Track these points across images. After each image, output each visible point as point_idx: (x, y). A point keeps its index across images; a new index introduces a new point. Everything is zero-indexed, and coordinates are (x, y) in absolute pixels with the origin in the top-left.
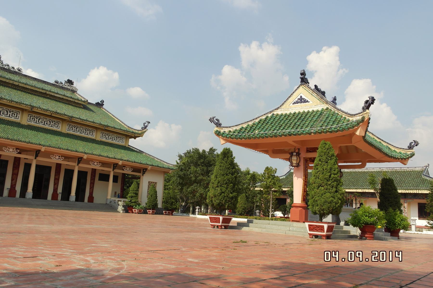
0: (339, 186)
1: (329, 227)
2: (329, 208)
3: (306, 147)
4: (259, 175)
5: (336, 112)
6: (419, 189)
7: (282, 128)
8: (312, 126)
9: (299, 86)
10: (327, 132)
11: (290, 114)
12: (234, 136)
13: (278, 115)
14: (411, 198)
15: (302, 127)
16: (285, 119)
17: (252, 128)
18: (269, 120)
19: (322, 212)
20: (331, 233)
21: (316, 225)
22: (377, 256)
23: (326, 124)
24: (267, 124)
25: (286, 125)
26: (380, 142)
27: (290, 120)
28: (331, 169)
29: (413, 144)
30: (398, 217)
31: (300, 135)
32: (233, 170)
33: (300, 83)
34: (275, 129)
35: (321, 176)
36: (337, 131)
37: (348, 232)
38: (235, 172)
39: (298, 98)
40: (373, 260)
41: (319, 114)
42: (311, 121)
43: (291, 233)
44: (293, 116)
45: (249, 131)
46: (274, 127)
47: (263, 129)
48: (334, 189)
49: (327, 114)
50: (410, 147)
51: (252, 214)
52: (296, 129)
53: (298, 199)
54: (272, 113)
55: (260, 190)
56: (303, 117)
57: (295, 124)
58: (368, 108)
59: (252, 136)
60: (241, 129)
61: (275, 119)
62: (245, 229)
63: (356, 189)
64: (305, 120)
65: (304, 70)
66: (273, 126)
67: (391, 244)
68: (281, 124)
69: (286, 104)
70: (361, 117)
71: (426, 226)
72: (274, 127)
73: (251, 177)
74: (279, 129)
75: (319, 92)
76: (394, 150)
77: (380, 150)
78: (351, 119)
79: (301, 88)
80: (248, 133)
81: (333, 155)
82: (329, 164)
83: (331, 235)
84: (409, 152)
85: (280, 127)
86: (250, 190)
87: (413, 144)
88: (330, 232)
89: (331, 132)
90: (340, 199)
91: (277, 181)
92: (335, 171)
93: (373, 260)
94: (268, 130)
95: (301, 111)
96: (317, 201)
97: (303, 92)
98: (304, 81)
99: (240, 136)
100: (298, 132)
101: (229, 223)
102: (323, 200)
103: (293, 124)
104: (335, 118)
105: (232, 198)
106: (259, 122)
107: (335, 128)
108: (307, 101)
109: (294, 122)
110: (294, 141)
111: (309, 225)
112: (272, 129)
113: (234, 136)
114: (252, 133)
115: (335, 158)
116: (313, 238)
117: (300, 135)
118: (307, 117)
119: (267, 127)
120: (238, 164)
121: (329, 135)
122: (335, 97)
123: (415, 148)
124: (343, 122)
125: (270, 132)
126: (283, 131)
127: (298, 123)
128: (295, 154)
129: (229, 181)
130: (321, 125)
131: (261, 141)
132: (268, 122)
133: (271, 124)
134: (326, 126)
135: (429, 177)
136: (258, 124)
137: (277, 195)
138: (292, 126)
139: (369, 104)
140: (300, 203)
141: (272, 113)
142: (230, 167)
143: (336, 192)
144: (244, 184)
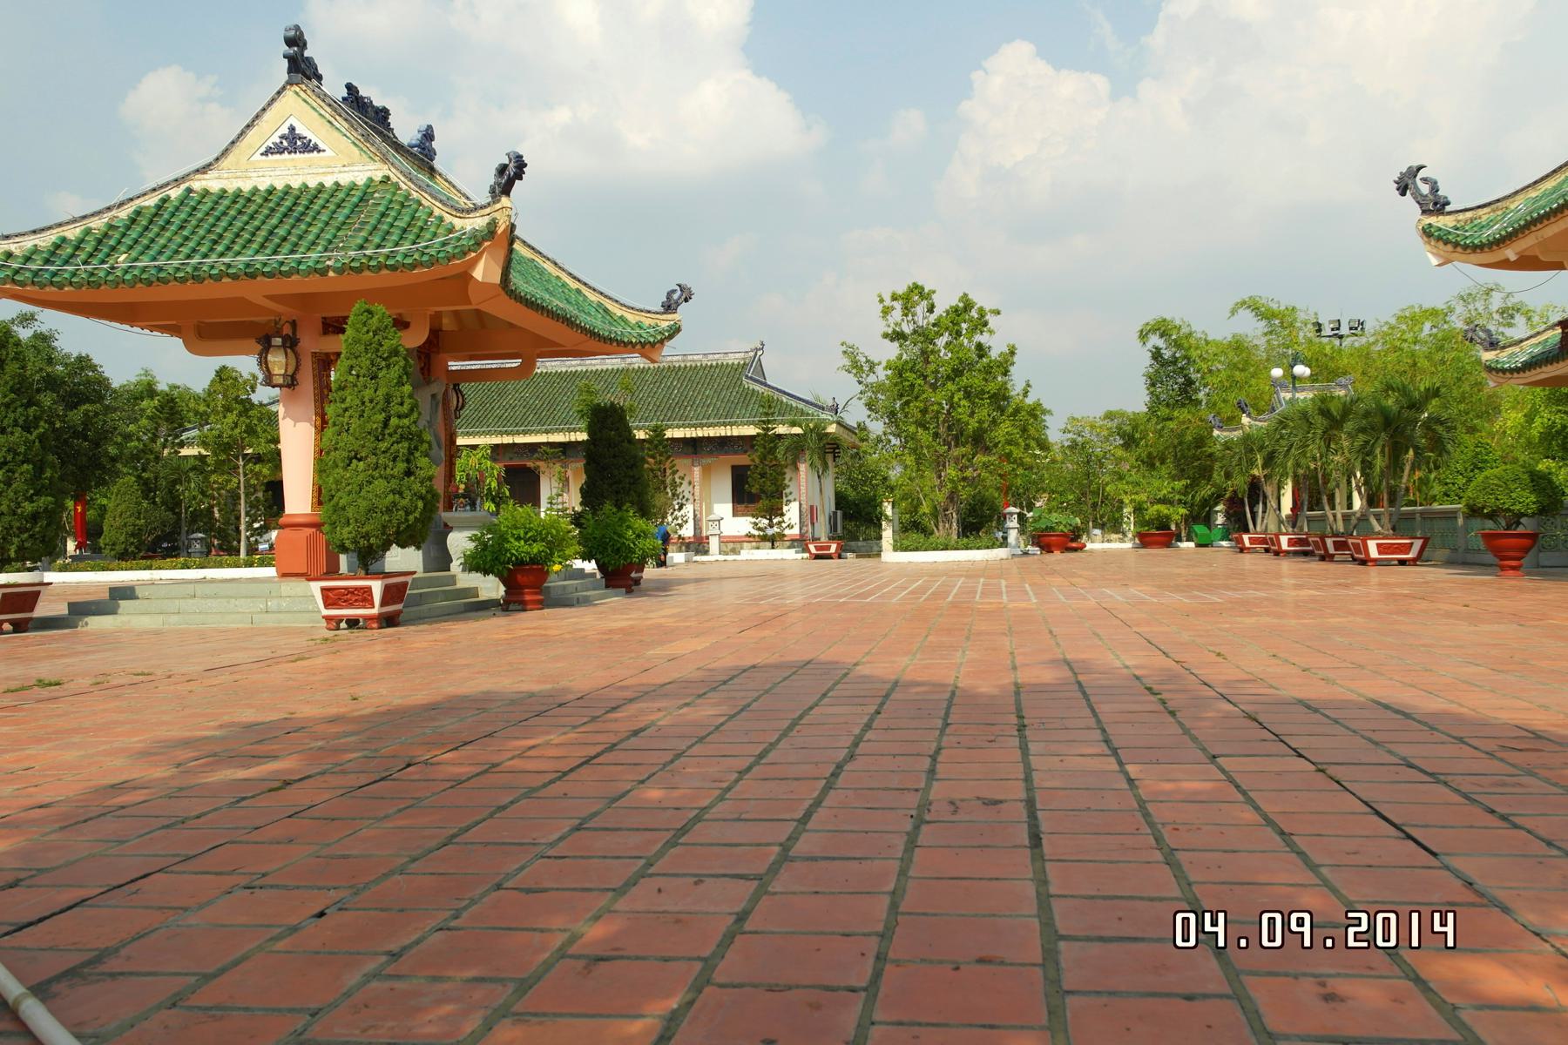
0: (417, 454)
1: (387, 590)
2: (384, 527)
3: (319, 316)
4: (197, 398)
5: (415, 195)
6: (731, 424)
7: (220, 248)
8: (330, 242)
9: (284, 88)
10: (380, 267)
11: (255, 191)
12: (28, 274)
13: (206, 193)
14: (711, 453)
15: (296, 245)
16: (232, 212)
17: (104, 243)
18: (173, 215)
19: (363, 542)
20: (399, 607)
21: (345, 588)
22: (1364, 927)
23: (377, 240)
24: (163, 228)
25: (238, 235)
26: (578, 291)
27: (252, 217)
28: (388, 399)
29: (675, 296)
30: (629, 527)
31: (288, 274)
32: (32, 410)
33: (285, 77)
34: (194, 251)
35: (355, 423)
36: (414, 266)
37: (473, 592)
38: (37, 419)
39: (279, 133)
40: (1351, 943)
41: (355, 200)
42: (327, 224)
43: (270, 621)
44: (266, 200)
45: (91, 255)
46: (192, 244)
47: (148, 247)
48: (401, 466)
49: (384, 202)
50: (669, 307)
51: (175, 548)
52: (275, 252)
53: (298, 499)
54: (183, 186)
55: (201, 458)
56: (300, 209)
57: (271, 233)
58: (506, 190)
59: (102, 274)
60: (57, 246)
61: (194, 209)
62: (95, 623)
63: (547, 432)
64: (308, 219)
65: (297, 28)
66: (187, 239)
67: (614, 613)
68: (219, 230)
69: (236, 151)
70: (487, 220)
71: (749, 535)
72: (192, 244)
73: (160, 409)
74: (212, 250)
75: (367, 116)
76: (621, 317)
77: (568, 321)
78: (458, 223)
79: (289, 93)
80: (85, 263)
81: (395, 352)
82: (382, 382)
83: (399, 613)
84: (665, 323)
85: (215, 242)
86: (157, 459)
87: (675, 296)
88: (394, 603)
89: (394, 268)
90: (422, 498)
91: (260, 420)
92: (402, 404)
93: (1351, 943)
94: (168, 253)
95: (296, 184)
96: (343, 509)
97: (296, 111)
98: (301, 68)
99: (55, 274)
100: (282, 263)
101: (32, 610)
102: (363, 504)
103: (263, 233)
104: (407, 219)
105: (35, 517)
106: (133, 221)
107: (406, 256)
108: (316, 148)
109: (266, 227)
110: (271, 298)
111: (323, 589)
112: (185, 250)
113: (28, 274)
114: (103, 262)
115: (402, 363)
116: (338, 628)
117: (288, 274)
118: (316, 207)
119: (162, 241)
120: (95, 361)
121: (386, 279)
122: (430, 127)
123: (683, 307)
124: (435, 235)
125: (175, 263)
126: (226, 260)
127: (281, 232)
128: (278, 341)
129: (16, 454)
130: (359, 241)
131: (141, 294)
132: (168, 222)
133: (182, 228)
134: (379, 246)
135: (765, 385)
136: (128, 228)
137: (265, 471)
138: (259, 240)
139: (510, 175)
140: (309, 510)
141: (183, 186)
142: (13, 401)
143: (409, 473)
144: (128, 437)
